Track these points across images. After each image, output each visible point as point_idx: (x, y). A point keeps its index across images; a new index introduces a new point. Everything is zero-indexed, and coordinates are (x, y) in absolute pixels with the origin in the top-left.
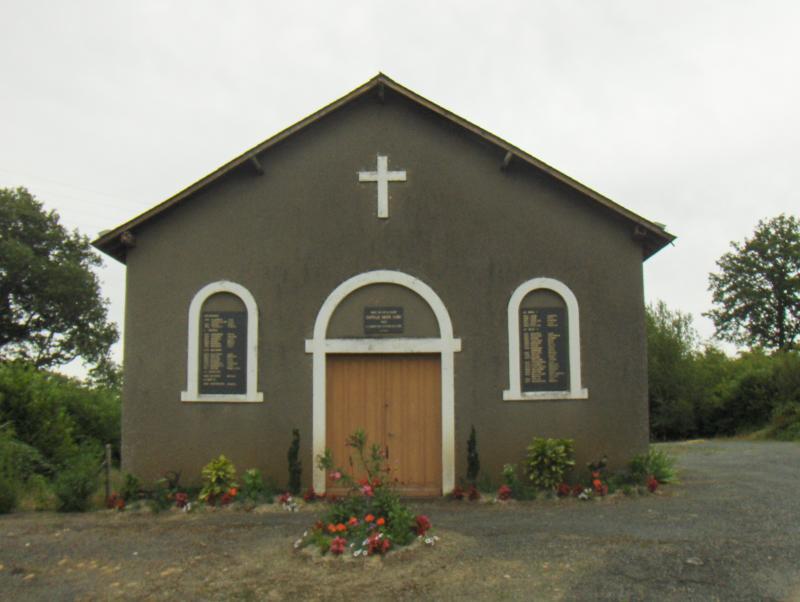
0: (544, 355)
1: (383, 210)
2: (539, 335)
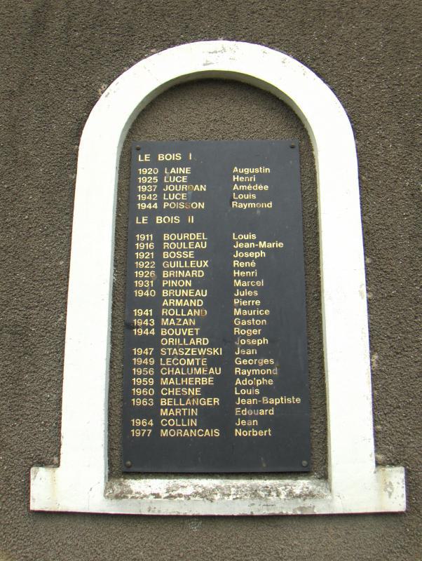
0: (217, 324)
2: (199, 240)
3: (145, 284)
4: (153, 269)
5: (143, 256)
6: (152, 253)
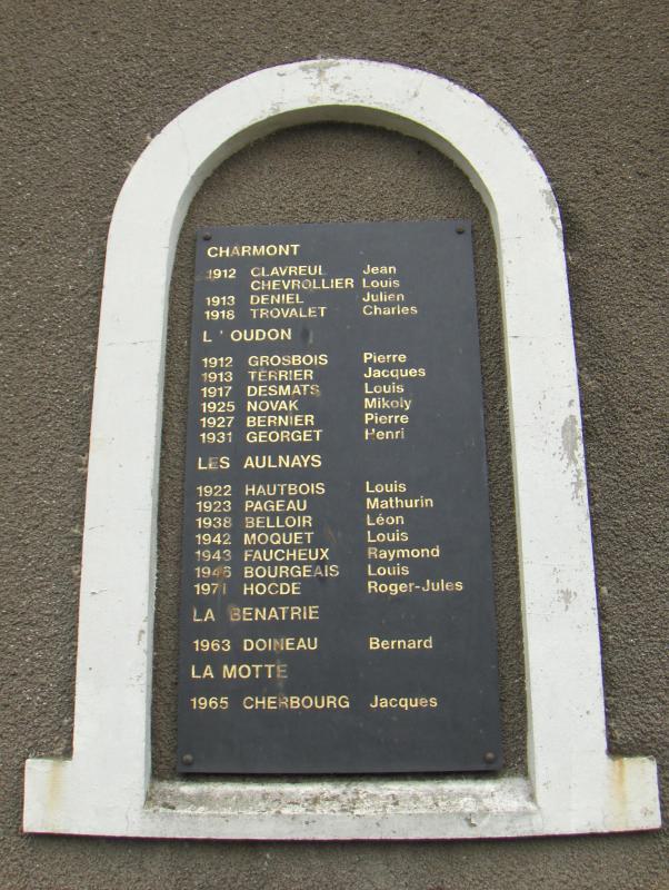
1: (429, 502)
3: (218, 437)
4: (227, 498)
5: (215, 407)
6: (230, 434)
